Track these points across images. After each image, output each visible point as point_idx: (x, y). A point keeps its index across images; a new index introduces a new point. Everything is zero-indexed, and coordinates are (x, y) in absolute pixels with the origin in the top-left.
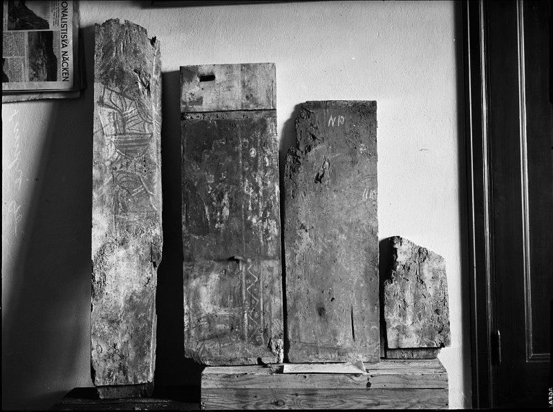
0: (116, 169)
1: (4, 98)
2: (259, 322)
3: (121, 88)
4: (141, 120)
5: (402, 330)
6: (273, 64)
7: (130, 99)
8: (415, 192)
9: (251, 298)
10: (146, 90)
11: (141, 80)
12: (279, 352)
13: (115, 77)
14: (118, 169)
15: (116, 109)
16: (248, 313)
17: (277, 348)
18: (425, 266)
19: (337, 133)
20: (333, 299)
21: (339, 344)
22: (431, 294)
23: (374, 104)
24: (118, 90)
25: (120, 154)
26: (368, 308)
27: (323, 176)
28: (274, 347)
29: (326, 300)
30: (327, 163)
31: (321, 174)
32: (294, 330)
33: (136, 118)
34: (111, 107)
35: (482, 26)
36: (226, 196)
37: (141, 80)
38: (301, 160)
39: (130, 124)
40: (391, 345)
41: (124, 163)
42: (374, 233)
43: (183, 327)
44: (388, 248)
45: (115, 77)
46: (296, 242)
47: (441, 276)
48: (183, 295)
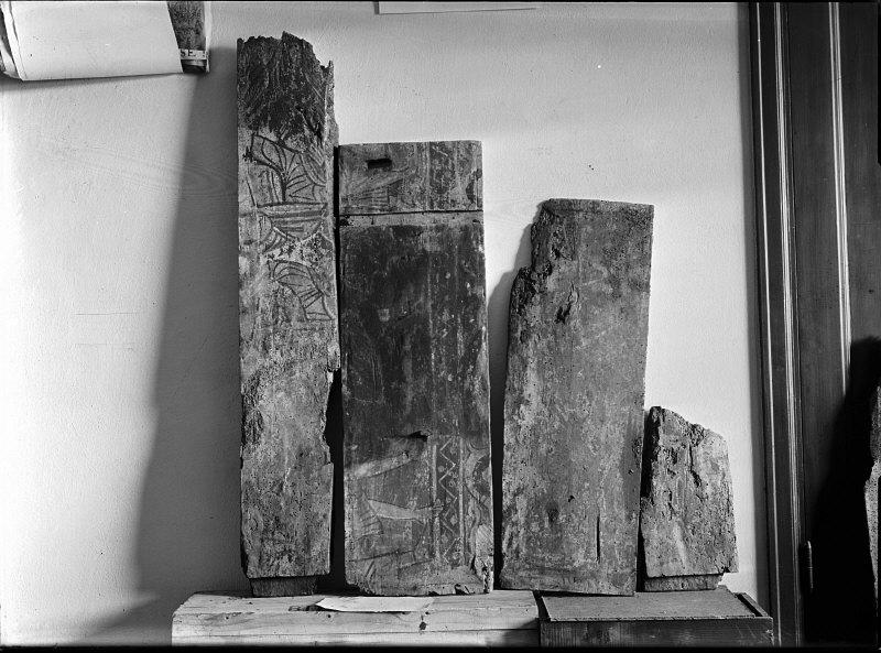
0: (272, 257)
1: (746, 4)
2: (457, 531)
3: (278, 135)
4: (309, 182)
5: (668, 551)
6: (470, 144)
7: (291, 150)
8: (693, 348)
9: (446, 495)
10: (316, 137)
11: (308, 122)
12: (488, 575)
13: (269, 118)
14: (276, 257)
15: (271, 167)
16: (441, 517)
17: (484, 569)
18: (700, 450)
19: (592, 244)
20: (572, 497)
21: (576, 564)
22: (709, 494)
23: (651, 208)
24: (274, 139)
25: (277, 234)
26: (623, 514)
27: (567, 312)
28: (479, 569)
29: (561, 498)
30: (575, 294)
31: (565, 308)
32: (511, 540)
33: (302, 179)
34: (264, 164)
35: (781, 88)
36: (407, 341)
37: (308, 122)
38: (536, 287)
39: (293, 189)
40: (652, 572)
41: (286, 248)
42: (639, 399)
43: (344, 538)
44: (653, 423)
45: (269, 118)
46: (522, 407)
47: (722, 466)
48: (343, 490)
